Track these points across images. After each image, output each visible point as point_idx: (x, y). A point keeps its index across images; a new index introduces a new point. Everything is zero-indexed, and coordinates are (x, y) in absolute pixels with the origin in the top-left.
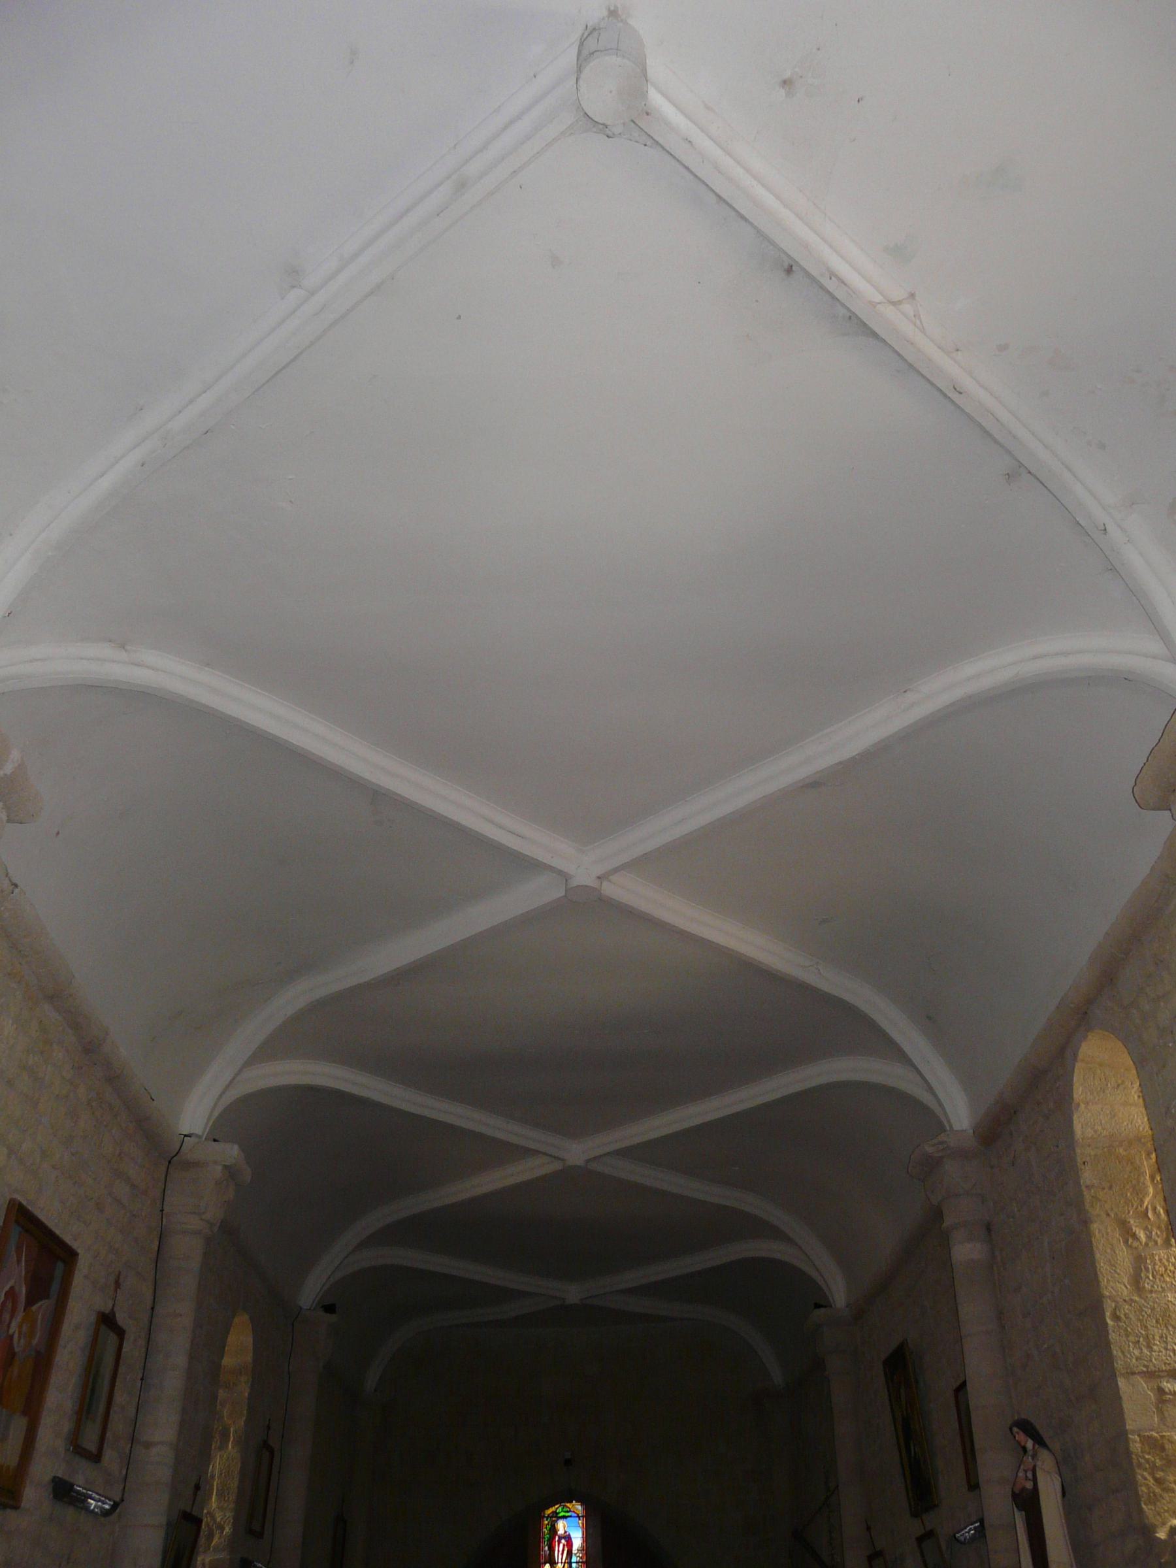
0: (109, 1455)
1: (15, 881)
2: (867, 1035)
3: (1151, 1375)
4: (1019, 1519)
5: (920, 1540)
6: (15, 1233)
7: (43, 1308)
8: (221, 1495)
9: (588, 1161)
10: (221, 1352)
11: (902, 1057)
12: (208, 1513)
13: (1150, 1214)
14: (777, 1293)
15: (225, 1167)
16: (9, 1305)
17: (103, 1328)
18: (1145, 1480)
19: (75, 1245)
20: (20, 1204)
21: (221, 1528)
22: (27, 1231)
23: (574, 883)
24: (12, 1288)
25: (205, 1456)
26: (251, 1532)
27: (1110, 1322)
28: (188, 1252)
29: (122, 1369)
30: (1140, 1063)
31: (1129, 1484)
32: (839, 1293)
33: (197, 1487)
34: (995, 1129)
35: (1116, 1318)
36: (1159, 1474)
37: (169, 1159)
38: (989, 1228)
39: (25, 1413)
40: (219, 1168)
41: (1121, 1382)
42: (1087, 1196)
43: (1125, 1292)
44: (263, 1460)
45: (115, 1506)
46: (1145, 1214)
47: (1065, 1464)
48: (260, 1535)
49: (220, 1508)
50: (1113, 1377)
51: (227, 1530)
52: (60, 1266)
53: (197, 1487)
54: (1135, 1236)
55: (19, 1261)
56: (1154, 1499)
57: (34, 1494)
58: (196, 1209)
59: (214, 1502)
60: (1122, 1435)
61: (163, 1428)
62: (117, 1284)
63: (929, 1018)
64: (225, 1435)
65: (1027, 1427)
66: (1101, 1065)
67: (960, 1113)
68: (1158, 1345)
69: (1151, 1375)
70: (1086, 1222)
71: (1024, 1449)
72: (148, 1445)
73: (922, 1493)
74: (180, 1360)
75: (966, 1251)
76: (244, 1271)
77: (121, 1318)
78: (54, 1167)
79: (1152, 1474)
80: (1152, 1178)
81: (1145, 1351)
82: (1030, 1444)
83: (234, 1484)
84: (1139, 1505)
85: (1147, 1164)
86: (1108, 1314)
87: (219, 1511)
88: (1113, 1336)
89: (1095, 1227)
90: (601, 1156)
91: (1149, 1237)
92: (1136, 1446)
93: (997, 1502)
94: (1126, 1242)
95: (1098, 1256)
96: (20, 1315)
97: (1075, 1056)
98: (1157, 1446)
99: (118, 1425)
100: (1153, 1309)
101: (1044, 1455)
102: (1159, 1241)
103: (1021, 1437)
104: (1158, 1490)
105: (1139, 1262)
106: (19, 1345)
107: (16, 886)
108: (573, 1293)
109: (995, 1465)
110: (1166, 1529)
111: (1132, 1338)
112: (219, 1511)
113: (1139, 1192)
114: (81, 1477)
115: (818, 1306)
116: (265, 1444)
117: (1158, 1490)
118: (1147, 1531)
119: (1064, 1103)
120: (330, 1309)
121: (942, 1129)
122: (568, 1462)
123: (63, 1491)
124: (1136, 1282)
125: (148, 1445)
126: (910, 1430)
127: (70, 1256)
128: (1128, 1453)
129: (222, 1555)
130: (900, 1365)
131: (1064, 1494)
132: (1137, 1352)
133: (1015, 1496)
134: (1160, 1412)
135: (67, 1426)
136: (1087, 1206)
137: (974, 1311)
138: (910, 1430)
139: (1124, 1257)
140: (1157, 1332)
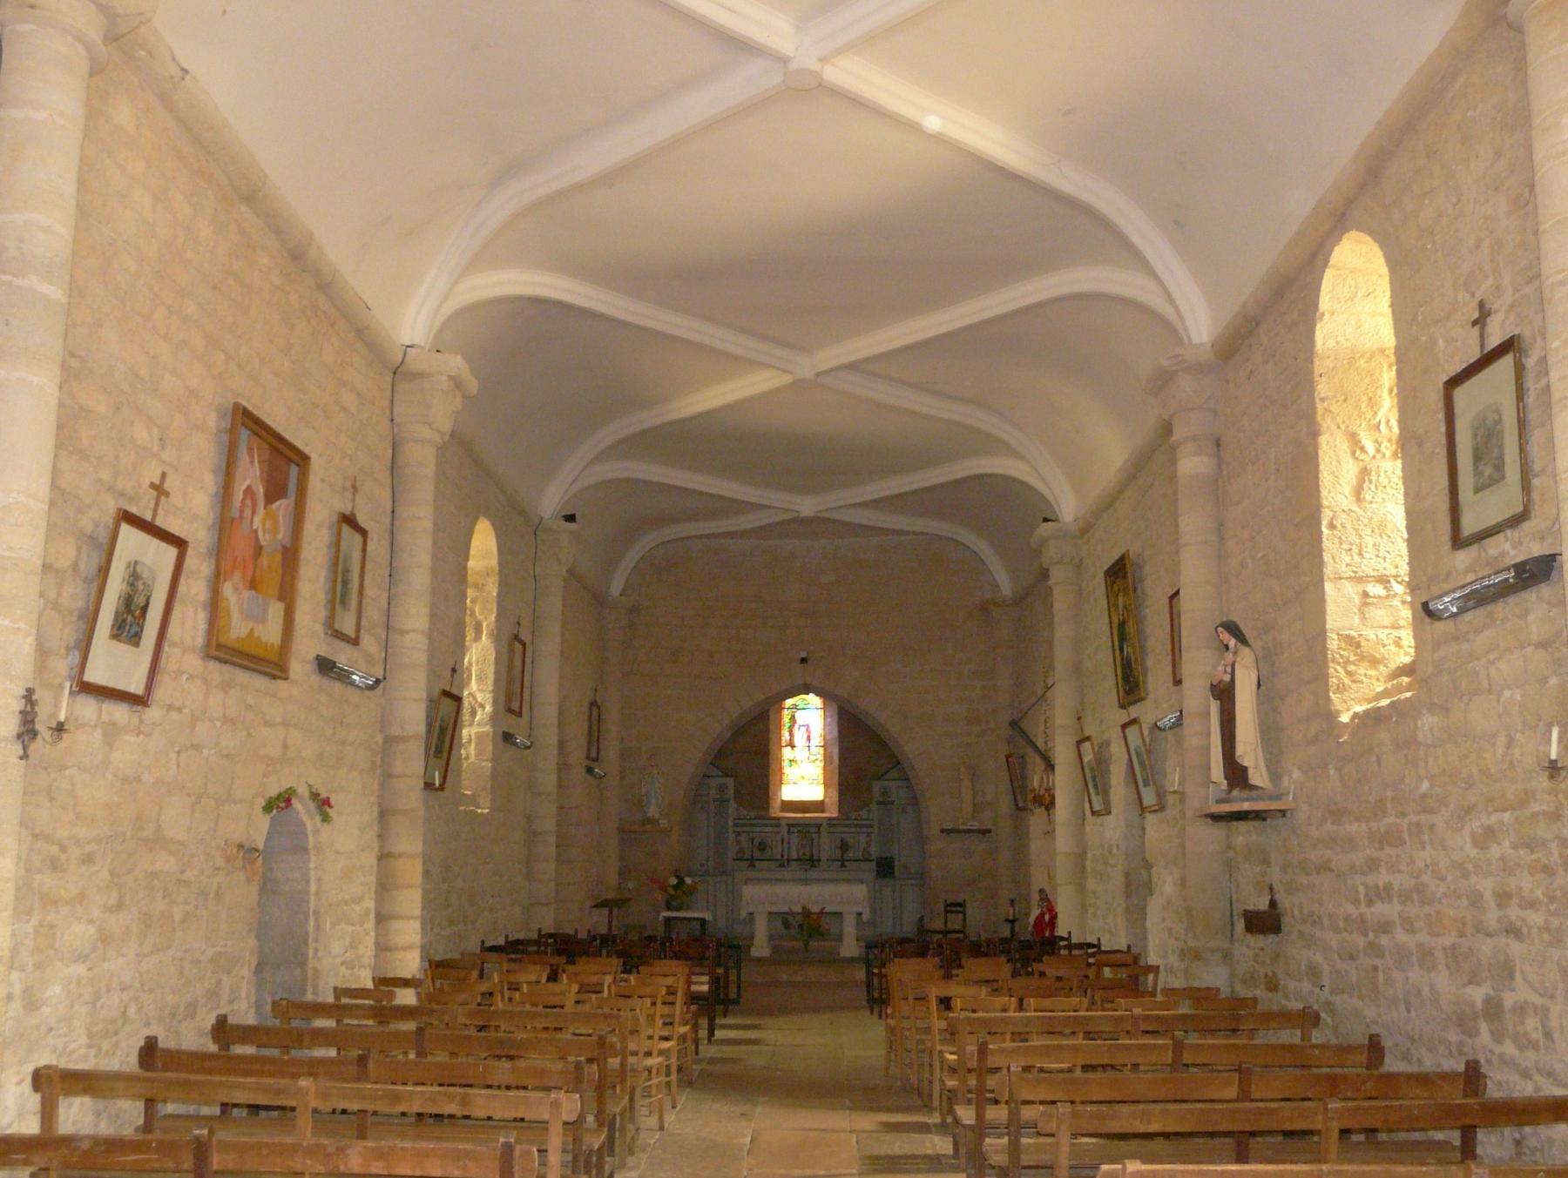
0: (366, 640)
1: (185, 66)
2: (1112, 242)
3: (1358, 579)
4: (1214, 706)
5: (1124, 727)
6: (244, 434)
7: (283, 506)
8: (480, 679)
9: (818, 375)
10: (467, 557)
11: (1139, 260)
12: (470, 694)
13: (1383, 427)
14: (1007, 509)
15: (451, 378)
16: (249, 502)
17: (346, 529)
18: (1337, 673)
19: (306, 450)
20: (245, 409)
21: (482, 706)
22: (257, 434)
23: (794, 65)
24: (249, 487)
25: (460, 647)
26: (510, 711)
27: (1325, 530)
28: (423, 460)
29: (368, 566)
30: (1394, 265)
31: (1322, 677)
32: (1069, 508)
33: (454, 670)
34: (1237, 341)
35: (1332, 526)
36: (1351, 668)
37: (399, 373)
38: (1218, 443)
39: (281, 598)
40: (444, 378)
41: (1328, 586)
42: (1320, 407)
43: (1345, 502)
44: (516, 651)
45: (378, 682)
46: (1377, 427)
47: (1265, 660)
48: (520, 714)
49: (481, 691)
50: (1322, 581)
51: (488, 708)
52: (294, 470)
53: (454, 670)
54: (1362, 449)
55: (252, 462)
56: (1341, 689)
57: (300, 668)
58: (433, 418)
59: (474, 685)
60: (1321, 634)
61: (415, 618)
62: (355, 489)
63: (1176, 222)
64: (478, 628)
65: (1233, 629)
66: (1352, 271)
67: (1201, 324)
68: (1369, 552)
69: (1358, 579)
70: (1315, 434)
71: (1227, 647)
72: (402, 633)
73: (1131, 686)
74: (425, 559)
75: (1192, 464)
76: (478, 478)
77: (361, 520)
78: (275, 374)
79: (1345, 668)
80: (1391, 391)
81: (1356, 557)
82: (1232, 642)
83: (491, 670)
84: (1327, 692)
85: (1388, 377)
86: (1324, 523)
87: (479, 693)
88: (1326, 543)
89: (1323, 439)
90: (831, 370)
91: (1378, 451)
92: (1333, 642)
93: (1196, 694)
94: (1353, 453)
95: (1322, 467)
96: (261, 511)
97: (1326, 262)
98: (1353, 643)
99: (373, 614)
100: (1370, 519)
101: (1245, 651)
102: (1388, 454)
103: (1225, 636)
104: (1347, 681)
105: (1365, 471)
106: (264, 539)
107: (186, 71)
108: (807, 506)
109: (1200, 666)
110: (1351, 713)
111: (1345, 546)
112: (479, 693)
113: (1373, 404)
114: (343, 656)
115: (1046, 520)
116: (517, 638)
117: (1347, 681)
118: (1331, 716)
119: (1308, 313)
120: (570, 518)
121: (1179, 341)
122: (804, 660)
123: (325, 666)
124: (1358, 493)
125: (402, 633)
126: (1124, 633)
127: (305, 458)
128: (1324, 649)
129: (487, 729)
130: (1119, 572)
131: (1259, 685)
132: (1348, 559)
133: (1213, 686)
134: (1362, 613)
135: (323, 614)
136: (1319, 418)
137: (1193, 522)
138: (1124, 633)
139: (1349, 470)
140: (1369, 541)
